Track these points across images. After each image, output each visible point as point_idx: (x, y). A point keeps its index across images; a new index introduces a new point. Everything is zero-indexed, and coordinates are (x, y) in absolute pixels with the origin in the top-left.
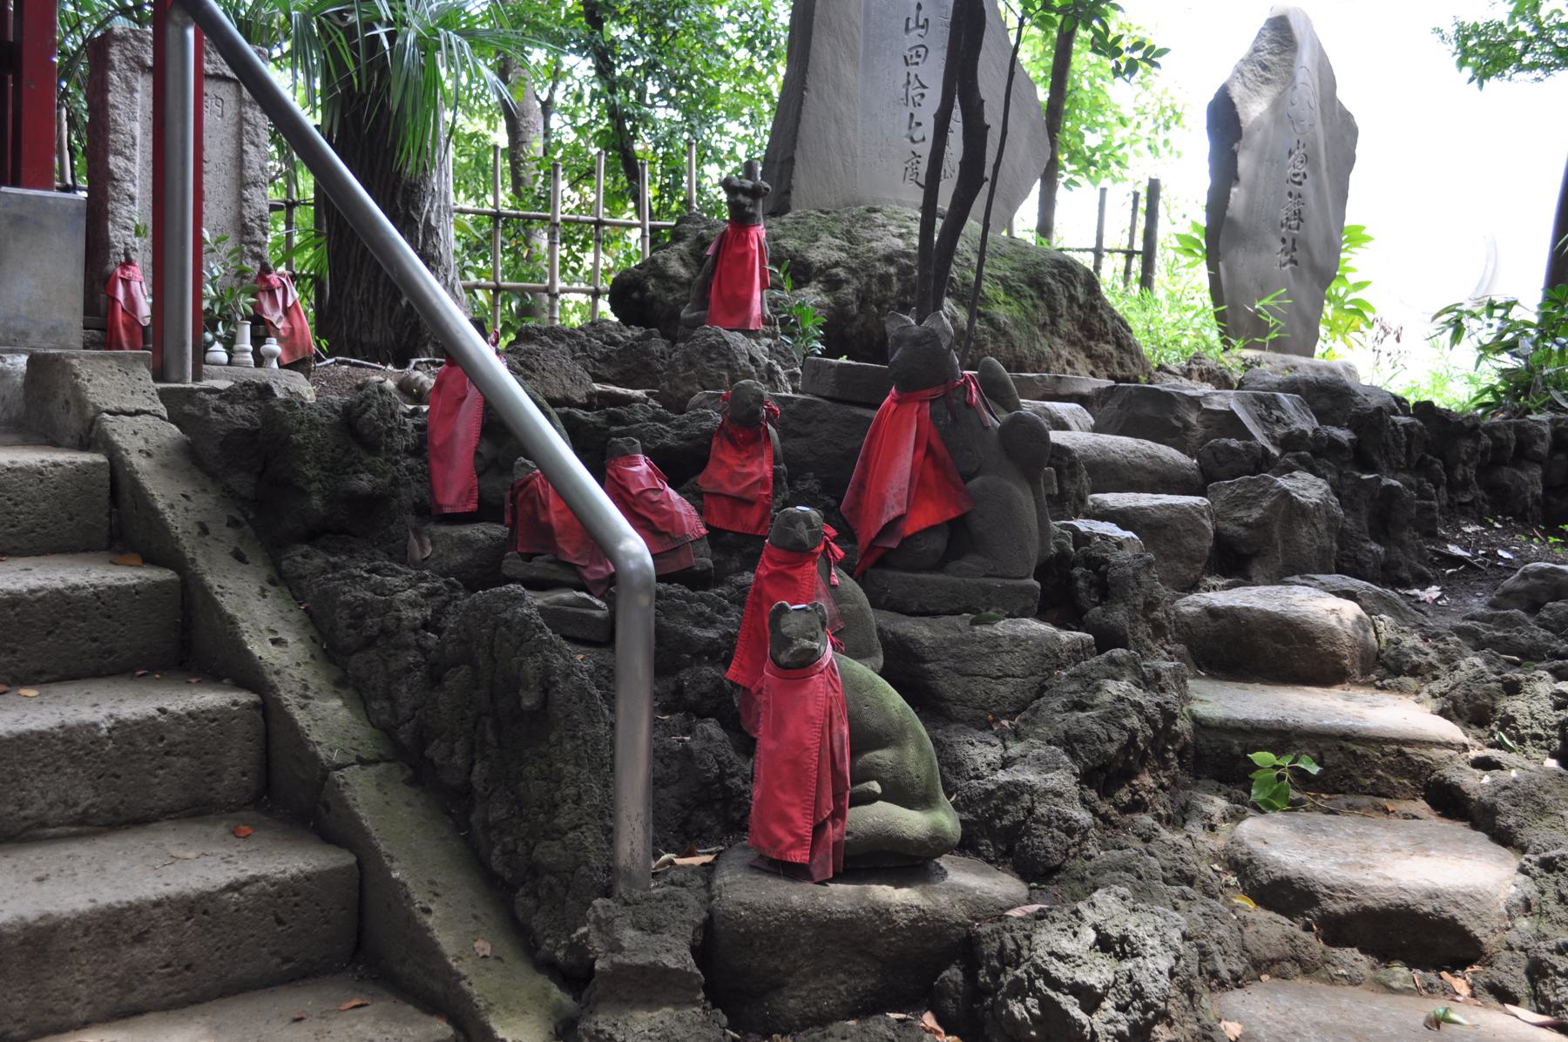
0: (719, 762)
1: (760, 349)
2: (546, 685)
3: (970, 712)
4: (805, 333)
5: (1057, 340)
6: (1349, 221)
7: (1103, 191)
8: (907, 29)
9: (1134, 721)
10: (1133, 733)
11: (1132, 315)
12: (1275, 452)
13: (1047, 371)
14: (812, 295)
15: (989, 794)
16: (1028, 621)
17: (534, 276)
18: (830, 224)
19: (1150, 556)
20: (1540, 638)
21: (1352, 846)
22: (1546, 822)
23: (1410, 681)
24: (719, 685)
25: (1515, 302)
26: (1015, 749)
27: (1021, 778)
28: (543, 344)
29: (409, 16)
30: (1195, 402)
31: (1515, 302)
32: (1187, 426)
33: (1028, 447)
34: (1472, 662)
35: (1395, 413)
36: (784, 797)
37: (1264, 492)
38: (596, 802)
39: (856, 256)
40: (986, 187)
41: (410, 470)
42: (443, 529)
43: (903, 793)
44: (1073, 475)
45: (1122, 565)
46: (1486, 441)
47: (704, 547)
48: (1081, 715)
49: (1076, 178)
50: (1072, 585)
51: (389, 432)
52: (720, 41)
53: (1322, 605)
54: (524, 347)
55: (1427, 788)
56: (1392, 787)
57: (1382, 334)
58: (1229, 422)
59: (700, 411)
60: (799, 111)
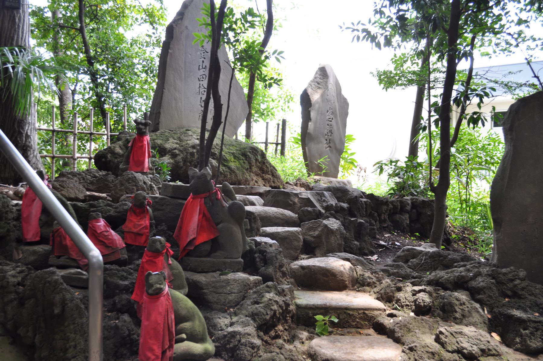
0: (129, 330)
1: (147, 179)
2: (64, 304)
3: (219, 306)
4: (164, 173)
5: (252, 174)
6: (347, 133)
7: (267, 123)
8: (199, 69)
9: (275, 307)
10: (275, 311)
11: (278, 165)
12: (323, 211)
13: (249, 185)
14: (167, 159)
15: (225, 336)
16: (239, 273)
17: (68, 152)
18: (173, 135)
19: (281, 249)
20: (408, 272)
21: (348, 346)
22: (411, 334)
23: (367, 288)
24: (129, 301)
25: (399, 160)
26: (235, 319)
27: (236, 329)
28: (69, 178)
29: (20, 60)
30: (296, 195)
31: (399, 160)
32: (294, 203)
33: (238, 213)
34: (387, 281)
35: (362, 197)
36: (151, 342)
37: (319, 226)
38: (82, 347)
39: (182, 146)
40: (222, 125)
41: (15, 226)
42: (27, 248)
43: (194, 338)
44: (255, 222)
45: (271, 253)
46: (391, 206)
47: (125, 251)
48: (257, 306)
49: (258, 119)
50: (255, 260)
51: (6, 213)
52: (136, 70)
53: (338, 264)
54: (61, 179)
55: (373, 324)
56: (362, 325)
57: (360, 170)
58: (308, 202)
59: (124, 202)
60: (162, 96)
